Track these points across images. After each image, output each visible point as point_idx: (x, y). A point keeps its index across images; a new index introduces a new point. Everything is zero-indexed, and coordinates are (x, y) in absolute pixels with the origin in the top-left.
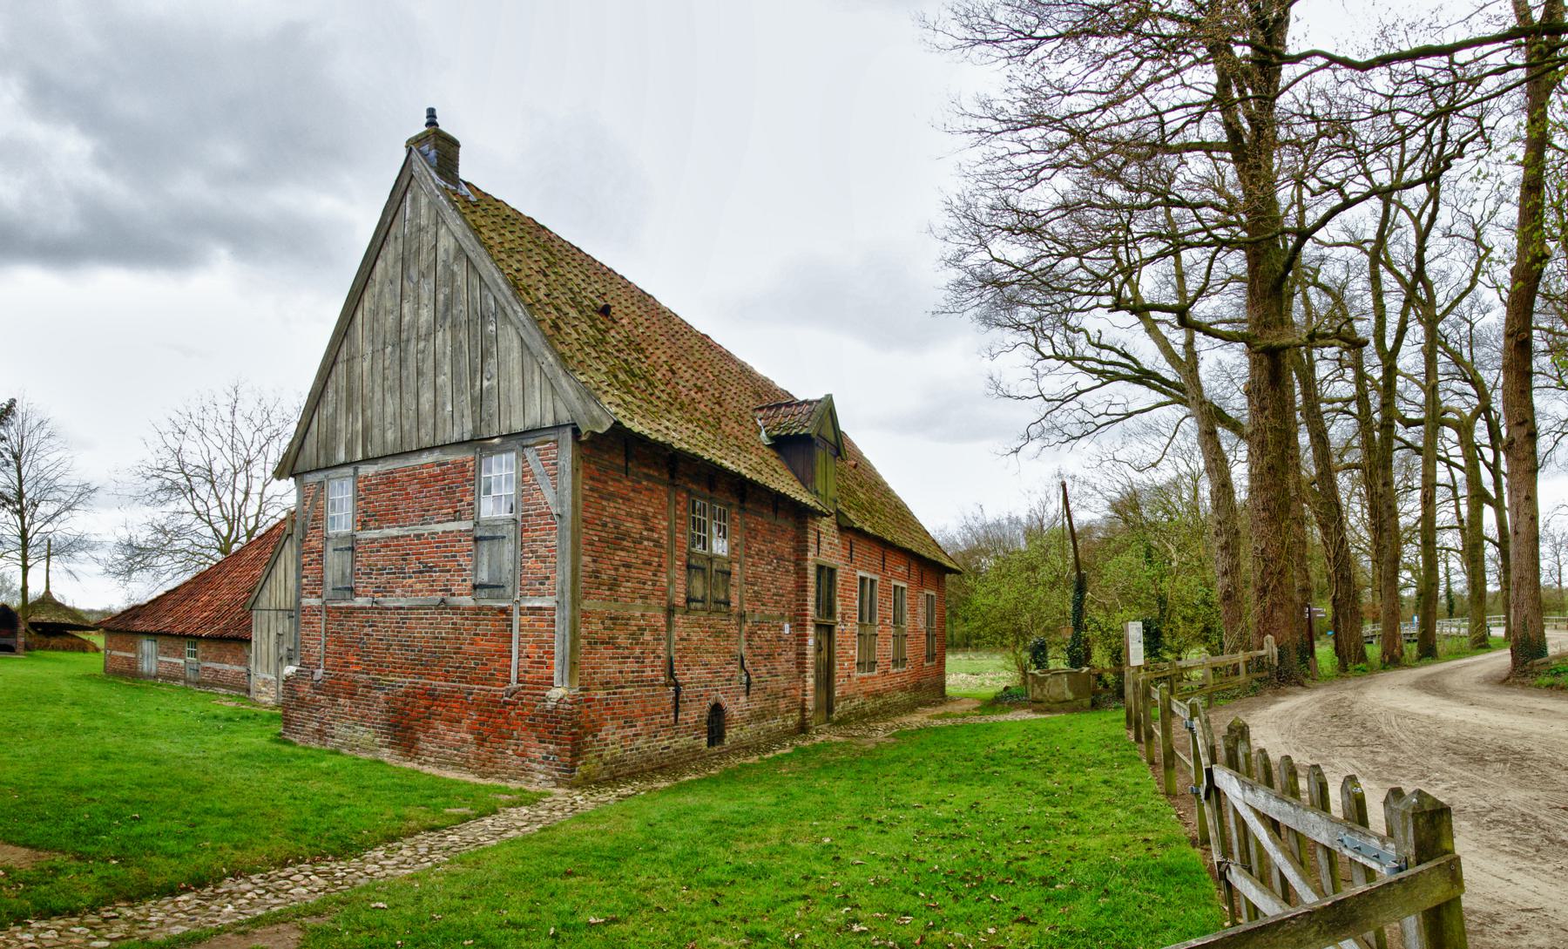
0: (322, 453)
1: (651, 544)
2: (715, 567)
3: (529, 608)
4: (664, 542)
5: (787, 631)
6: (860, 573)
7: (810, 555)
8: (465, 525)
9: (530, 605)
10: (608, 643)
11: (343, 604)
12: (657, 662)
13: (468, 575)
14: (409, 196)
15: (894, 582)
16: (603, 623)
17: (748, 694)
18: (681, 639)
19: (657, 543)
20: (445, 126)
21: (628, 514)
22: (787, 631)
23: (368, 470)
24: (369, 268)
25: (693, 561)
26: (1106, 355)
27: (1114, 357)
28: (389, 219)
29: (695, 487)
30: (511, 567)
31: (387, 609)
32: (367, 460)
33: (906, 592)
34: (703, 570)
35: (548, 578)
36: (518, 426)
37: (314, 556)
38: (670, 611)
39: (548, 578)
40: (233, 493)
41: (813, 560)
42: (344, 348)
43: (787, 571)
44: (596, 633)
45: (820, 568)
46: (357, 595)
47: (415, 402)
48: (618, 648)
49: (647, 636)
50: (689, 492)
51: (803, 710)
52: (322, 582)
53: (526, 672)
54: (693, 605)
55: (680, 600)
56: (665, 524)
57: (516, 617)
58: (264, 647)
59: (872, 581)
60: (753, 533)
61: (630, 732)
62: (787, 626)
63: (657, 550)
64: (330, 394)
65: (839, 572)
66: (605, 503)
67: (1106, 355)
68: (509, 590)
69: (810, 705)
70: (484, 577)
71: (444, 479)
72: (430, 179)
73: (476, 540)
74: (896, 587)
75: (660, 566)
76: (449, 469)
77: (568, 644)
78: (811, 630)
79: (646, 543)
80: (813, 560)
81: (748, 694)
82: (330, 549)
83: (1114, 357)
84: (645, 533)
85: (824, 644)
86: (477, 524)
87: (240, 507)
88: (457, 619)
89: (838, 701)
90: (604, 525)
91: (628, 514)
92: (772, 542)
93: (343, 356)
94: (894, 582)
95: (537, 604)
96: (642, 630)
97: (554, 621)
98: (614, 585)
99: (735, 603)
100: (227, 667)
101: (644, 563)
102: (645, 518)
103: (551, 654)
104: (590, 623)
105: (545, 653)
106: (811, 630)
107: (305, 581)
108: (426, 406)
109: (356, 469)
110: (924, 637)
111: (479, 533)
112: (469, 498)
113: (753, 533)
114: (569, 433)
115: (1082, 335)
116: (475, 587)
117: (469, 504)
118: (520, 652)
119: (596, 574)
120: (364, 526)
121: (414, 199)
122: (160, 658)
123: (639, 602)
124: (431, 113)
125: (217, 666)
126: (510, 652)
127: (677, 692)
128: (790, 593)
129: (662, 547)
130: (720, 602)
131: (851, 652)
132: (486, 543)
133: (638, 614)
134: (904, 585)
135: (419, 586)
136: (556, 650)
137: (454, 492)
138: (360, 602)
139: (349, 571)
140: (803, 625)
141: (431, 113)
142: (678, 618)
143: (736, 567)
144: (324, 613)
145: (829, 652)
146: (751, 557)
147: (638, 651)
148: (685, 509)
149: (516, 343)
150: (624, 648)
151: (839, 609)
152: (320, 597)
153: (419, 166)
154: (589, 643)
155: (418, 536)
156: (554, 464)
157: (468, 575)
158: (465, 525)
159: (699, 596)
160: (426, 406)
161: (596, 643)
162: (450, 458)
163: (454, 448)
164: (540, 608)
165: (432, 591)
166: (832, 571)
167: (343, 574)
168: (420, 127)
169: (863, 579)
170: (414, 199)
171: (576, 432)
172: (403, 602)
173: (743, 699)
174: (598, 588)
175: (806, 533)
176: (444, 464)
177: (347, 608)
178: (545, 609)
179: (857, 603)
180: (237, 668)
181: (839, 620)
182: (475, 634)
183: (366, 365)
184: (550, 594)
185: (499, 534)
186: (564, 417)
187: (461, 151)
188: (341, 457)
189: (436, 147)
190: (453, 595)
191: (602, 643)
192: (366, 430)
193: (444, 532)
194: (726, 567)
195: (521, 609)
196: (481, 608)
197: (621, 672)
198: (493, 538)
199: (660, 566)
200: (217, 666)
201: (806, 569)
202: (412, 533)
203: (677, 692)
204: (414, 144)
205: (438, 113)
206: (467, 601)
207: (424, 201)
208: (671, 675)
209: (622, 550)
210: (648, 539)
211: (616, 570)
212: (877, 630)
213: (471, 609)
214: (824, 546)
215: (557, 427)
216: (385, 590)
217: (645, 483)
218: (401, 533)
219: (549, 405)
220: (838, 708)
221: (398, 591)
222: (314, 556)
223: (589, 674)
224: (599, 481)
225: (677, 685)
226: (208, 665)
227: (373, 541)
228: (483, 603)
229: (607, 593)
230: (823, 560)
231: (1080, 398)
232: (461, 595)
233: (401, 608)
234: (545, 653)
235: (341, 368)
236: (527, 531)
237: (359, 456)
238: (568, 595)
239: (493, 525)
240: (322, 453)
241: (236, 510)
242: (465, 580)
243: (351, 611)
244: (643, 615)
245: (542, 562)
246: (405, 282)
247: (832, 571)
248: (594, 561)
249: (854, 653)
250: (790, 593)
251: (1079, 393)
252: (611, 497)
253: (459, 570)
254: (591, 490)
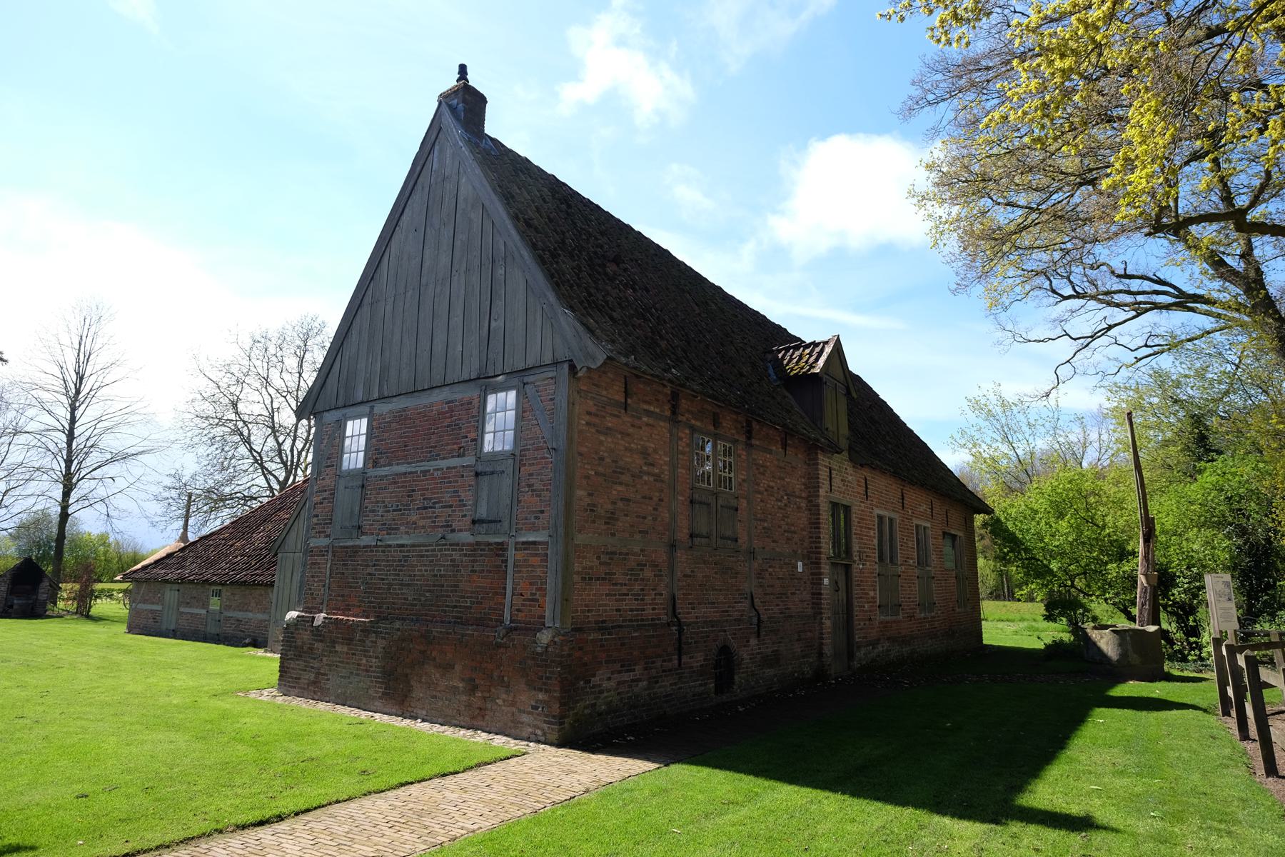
0: (342, 391)
1: (652, 479)
2: (720, 502)
3: (523, 543)
4: (666, 476)
5: (800, 570)
6: (877, 511)
7: (822, 492)
8: (469, 460)
9: (524, 539)
10: (604, 579)
11: (350, 543)
12: (660, 600)
13: (468, 510)
14: (437, 147)
15: (916, 522)
16: (598, 558)
17: (759, 636)
18: (685, 576)
19: (658, 478)
20: (474, 80)
21: (626, 449)
22: (800, 570)
23: (382, 408)
24: (397, 216)
25: (696, 496)
26: (1135, 285)
27: (1147, 286)
28: (419, 169)
29: (698, 424)
30: (508, 502)
31: (390, 546)
32: (382, 398)
33: (929, 532)
34: (708, 505)
35: (542, 512)
36: (521, 366)
37: (326, 494)
38: (673, 546)
39: (542, 512)
40: (294, 441)
41: (826, 497)
42: (370, 292)
43: (799, 508)
44: (591, 568)
45: (835, 506)
46: (363, 534)
47: (429, 344)
48: (616, 584)
49: (648, 573)
50: (693, 429)
51: (821, 654)
52: (330, 521)
53: (518, 610)
54: (697, 541)
55: (683, 535)
56: (667, 459)
57: (512, 554)
58: (286, 592)
59: (891, 520)
60: (761, 470)
61: (626, 677)
62: (800, 564)
63: (658, 485)
64: (354, 332)
65: (854, 509)
66: (602, 438)
67: (1135, 285)
68: (506, 524)
69: (828, 650)
70: (483, 512)
71: (451, 416)
72: (455, 132)
73: (477, 474)
74: (917, 526)
75: (661, 500)
76: (456, 406)
77: (560, 581)
78: (826, 568)
79: (645, 478)
80: (826, 497)
81: (759, 636)
82: (341, 487)
83: (1147, 286)
84: (645, 468)
85: (842, 585)
86: (478, 459)
87: (300, 454)
88: (456, 555)
89: (859, 647)
90: (602, 459)
91: (626, 449)
92: (783, 479)
93: (368, 299)
94: (916, 522)
95: (531, 539)
96: (642, 565)
97: (546, 555)
98: (611, 519)
99: (743, 538)
100: (250, 615)
101: (644, 497)
102: (644, 453)
103: (542, 590)
104: (585, 557)
105: (538, 589)
106: (826, 568)
107: (315, 520)
108: (439, 347)
109: (372, 408)
110: (954, 580)
111: (480, 469)
112: (472, 435)
113: (761, 470)
114: (566, 366)
115: (1104, 268)
116: (474, 522)
117: (472, 440)
118: (514, 589)
119: (591, 508)
120: (376, 464)
121: (441, 151)
122: (182, 609)
123: (638, 537)
124: (463, 69)
125: (239, 615)
126: (505, 588)
127: (680, 632)
128: (803, 530)
129: (662, 481)
130: (728, 538)
131: (872, 593)
132: (485, 478)
133: (637, 549)
134: (928, 525)
135: (421, 523)
136: (548, 587)
137: (460, 429)
138: (366, 540)
139: (357, 508)
140: (817, 563)
141: (463, 69)
142: (681, 555)
143: (744, 503)
144: (330, 554)
145: (847, 592)
146: (760, 493)
147: (637, 588)
148: (688, 445)
149: (522, 286)
150: (621, 585)
151: (855, 547)
152: (328, 536)
153: (448, 118)
154: (583, 579)
155: (424, 472)
156: (551, 399)
157: (468, 510)
158: (469, 460)
159: (704, 531)
160: (439, 347)
161: (591, 579)
162: (457, 396)
163: (461, 386)
164: (534, 543)
165: (433, 527)
166: (847, 509)
167: (352, 512)
168: (451, 81)
169: (881, 518)
170: (441, 151)
171: (573, 368)
172: (405, 540)
173: (753, 642)
174: (594, 522)
175: (817, 469)
176: (452, 402)
177: (352, 546)
178: (540, 543)
179: (876, 542)
180: (260, 616)
181: (856, 559)
182: (472, 571)
183: (389, 308)
184: (544, 528)
185: (498, 469)
186: (563, 354)
187: (488, 105)
188: (360, 396)
189: (464, 101)
190: (453, 531)
191: (598, 579)
192: (385, 370)
193: (448, 468)
194: (734, 503)
195: (517, 543)
196: (478, 543)
197: (618, 610)
198: (492, 473)
199: (661, 500)
200: (239, 615)
201: (818, 506)
202: (419, 469)
203: (680, 632)
204: (445, 99)
205: (469, 71)
206: (466, 537)
207: (449, 152)
208: (674, 613)
209: (621, 484)
210: (648, 474)
211: (614, 503)
212: (900, 569)
213: (469, 544)
214: (837, 482)
215: (555, 363)
216: (391, 529)
217: (645, 419)
218: (409, 470)
219: (549, 342)
220: (860, 654)
221: (403, 528)
222: (326, 494)
223: (582, 611)
224: (596, 415)
225: (680, 624)
226: (230, 614)
227: (382, 478)
228: (480, 539)
229: (604, 527)
230: (836, 497)
231: (1112, 332)
232: (461, 530)
233: (403, 546)
234: (538, 589)
235: (366, 309)
236: (525, 465)
237: (376, 396)
238: (561, 530)
239: (494, 456)
240: (342, 391)
241: (296, 456)
242: (465, 516)
243: (355, 550)
244: (642, 550)
245: (537, 496)
246: (428, 229)
247: (847, 509)
248: (590, 495)
249: (875, 594)
250: (803, 530)
251: (1110, 328)
252: (608, 431)
253: (460, 506)
254: (588, 424)
